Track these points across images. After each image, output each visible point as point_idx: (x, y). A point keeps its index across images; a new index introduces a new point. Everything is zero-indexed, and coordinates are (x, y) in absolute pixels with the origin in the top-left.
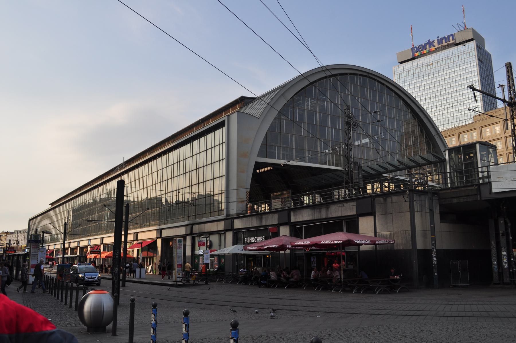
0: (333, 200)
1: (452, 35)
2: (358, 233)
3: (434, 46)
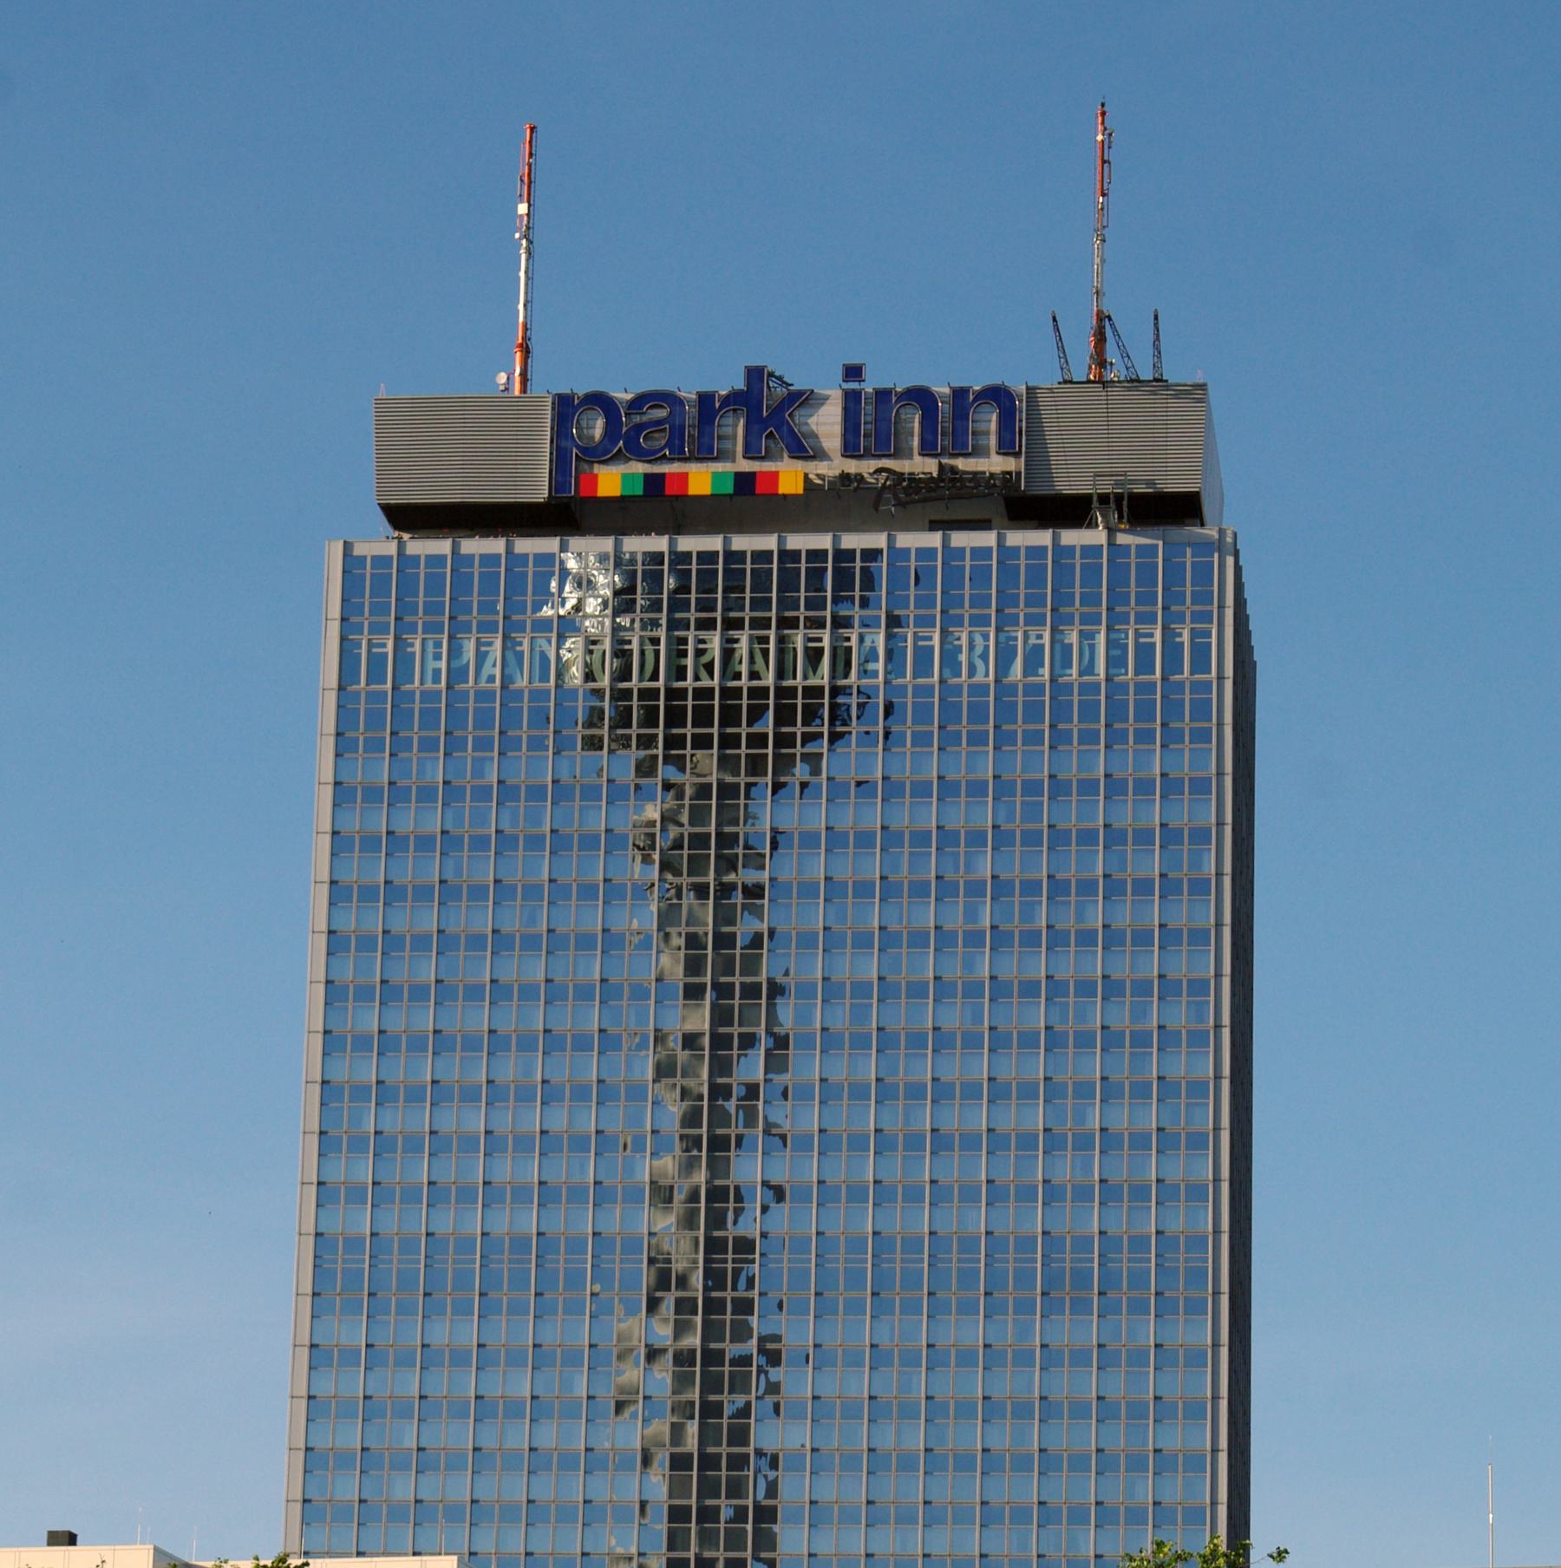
0: (1018, 474)
1: (998, 395)
2: (156, 1549)
3: (802, 448)
